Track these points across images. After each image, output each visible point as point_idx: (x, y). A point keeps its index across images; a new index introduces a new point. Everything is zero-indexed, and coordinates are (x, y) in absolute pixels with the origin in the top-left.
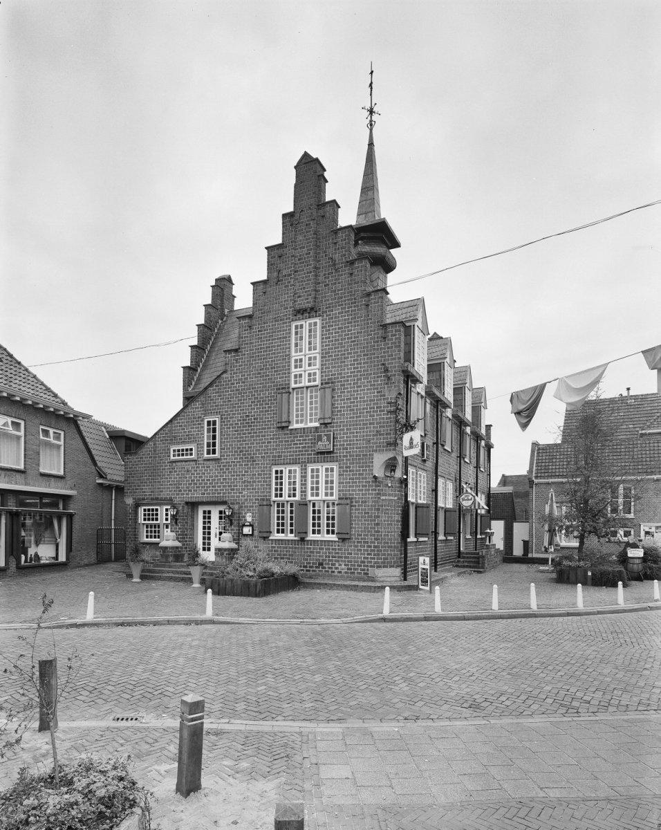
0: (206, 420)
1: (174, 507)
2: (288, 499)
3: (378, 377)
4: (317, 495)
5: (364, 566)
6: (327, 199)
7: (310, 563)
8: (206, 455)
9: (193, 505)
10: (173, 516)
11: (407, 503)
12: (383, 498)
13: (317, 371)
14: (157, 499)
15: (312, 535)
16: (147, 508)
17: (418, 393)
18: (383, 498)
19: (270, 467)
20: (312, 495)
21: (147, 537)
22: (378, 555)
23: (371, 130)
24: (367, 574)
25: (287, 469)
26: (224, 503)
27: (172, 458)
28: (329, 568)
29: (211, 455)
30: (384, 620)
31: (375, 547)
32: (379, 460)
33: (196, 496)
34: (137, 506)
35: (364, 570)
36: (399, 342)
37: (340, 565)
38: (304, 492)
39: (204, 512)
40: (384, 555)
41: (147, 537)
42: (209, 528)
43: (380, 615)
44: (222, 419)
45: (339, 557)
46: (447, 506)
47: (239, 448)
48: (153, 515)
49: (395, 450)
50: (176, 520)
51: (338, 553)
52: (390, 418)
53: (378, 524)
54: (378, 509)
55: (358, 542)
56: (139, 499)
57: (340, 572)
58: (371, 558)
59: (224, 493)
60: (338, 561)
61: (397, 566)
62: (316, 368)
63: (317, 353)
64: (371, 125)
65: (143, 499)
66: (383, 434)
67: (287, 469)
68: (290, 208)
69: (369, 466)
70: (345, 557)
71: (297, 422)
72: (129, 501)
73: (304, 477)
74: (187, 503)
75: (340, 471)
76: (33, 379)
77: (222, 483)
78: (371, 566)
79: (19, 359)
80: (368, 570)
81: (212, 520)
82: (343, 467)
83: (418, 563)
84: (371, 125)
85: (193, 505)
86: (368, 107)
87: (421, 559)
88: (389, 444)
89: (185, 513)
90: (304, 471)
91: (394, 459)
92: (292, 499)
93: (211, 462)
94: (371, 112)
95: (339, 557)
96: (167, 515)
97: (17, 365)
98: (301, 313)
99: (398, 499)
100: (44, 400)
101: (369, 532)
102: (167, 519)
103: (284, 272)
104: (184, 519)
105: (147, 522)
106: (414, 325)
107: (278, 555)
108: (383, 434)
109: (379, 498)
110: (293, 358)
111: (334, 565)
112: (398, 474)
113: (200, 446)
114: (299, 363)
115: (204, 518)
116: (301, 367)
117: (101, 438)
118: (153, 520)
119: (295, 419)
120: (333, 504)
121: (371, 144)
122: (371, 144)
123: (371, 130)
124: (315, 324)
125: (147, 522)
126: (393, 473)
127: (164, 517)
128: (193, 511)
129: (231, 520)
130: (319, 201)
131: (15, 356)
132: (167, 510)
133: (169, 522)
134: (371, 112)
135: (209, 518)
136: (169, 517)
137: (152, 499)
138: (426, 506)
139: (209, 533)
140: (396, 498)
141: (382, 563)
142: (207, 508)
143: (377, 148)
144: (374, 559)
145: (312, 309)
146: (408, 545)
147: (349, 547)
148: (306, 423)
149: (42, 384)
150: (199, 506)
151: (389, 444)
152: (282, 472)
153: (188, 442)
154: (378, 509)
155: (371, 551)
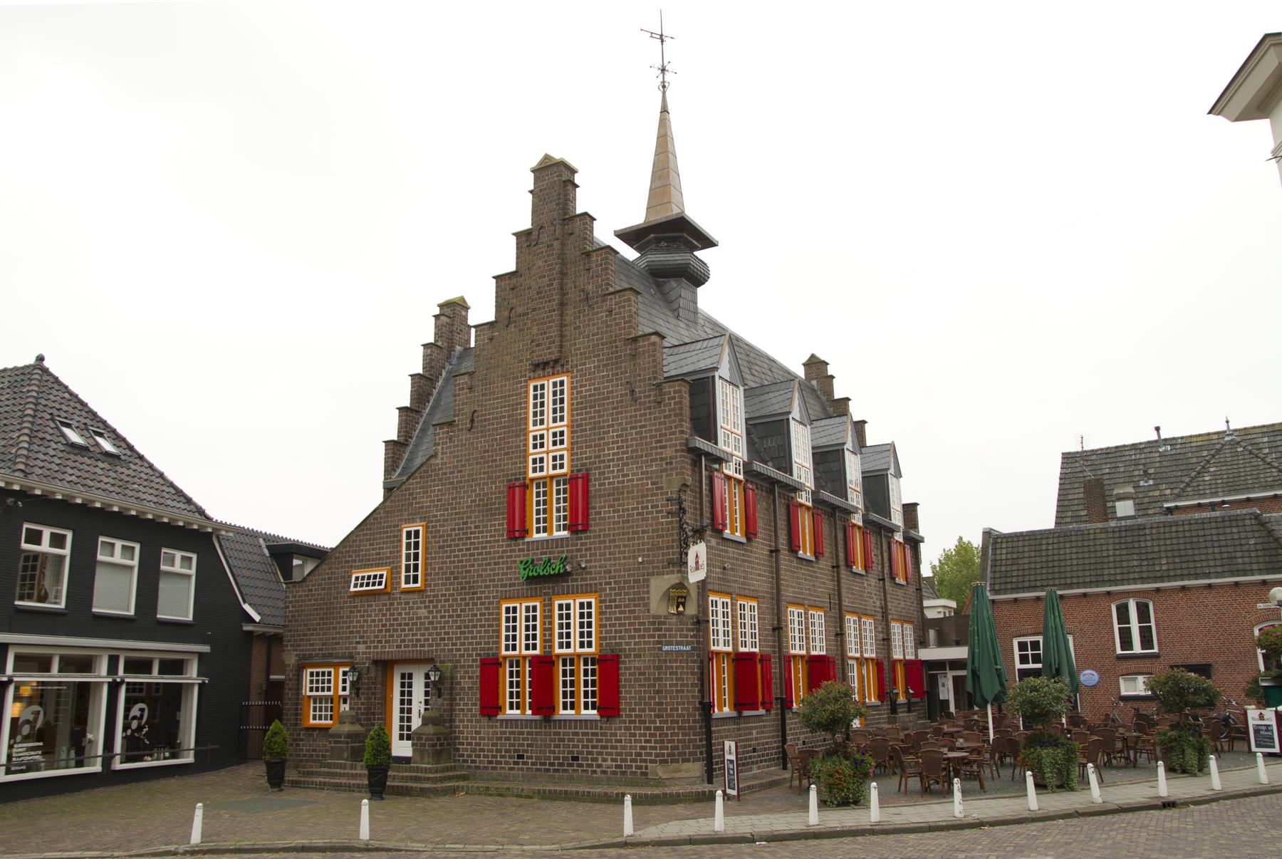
0: (405, 531)
1: (353, 669)
2: (579, 650)
3: (652, 461)
4: (514, 648)
5: (641, 761)
6: (578, 212)
7: (558, 758)
8: (404, 586)
9: (385, 666)
10: (352, 683)
11: (706, 658)
12: (666, 648)
13: (565, 453)
14: (331, 655)
15: (562, 712)
16: (315, 670)
17: (729, 478)
18: (666, 648)
19: (498, 603)
20: (561, 646)
21: (314, 718)
22: (662, 741)
23: (664, 93)
24: (644, 774)
25: (524, 605)
26: (430, 661)
27: (404, 586)
28: (588, 765)
29: (412, 585)
30: (625, 845)
31: (656, 729)
32: (659, 585)
33: (389, 650)
34: (300, 668)
35: (640, 767)
36: (681, 409)
37: (605, 760)
38: (548, 641)
39: (403, 676)
40: (672, 741)
41: (314, 718)
42: (410, 702)
43: (620, 840)
44: (428, 527)
45: (603, 747)
46: (908, 657)
47: (452, 573)
48: (317, 681)
49: (679, 572)
50: (358, 689)
51: (601, 741)
52: (671, 523)
53: (659, 692)
54: (659, 668)
55: (630, 722)
56: (305, 657)
57: (604, 772)
58: (651, 748)
59: (430, 645)
60: (601, 754)
61: (699, 760)
62: (563, 450)
63: (563, 426)
64: (664, 87)
65: (311, 656)
66: (662, 548)
67: (524, 605)
68: (526, 223)
69: (643, 599)
70: (612, 747)
71: (538, 531)
72: (291, 659)
73: (548, 617)
74: (375, 662)
75: (601, 607)
76: (159, 480)
77: (427, 629)
78: (652, 761)
79: (142, 452)
80: (646, 767)
81: (414, 689)
82: (604, 601)
83: (723, 749)
84: (664, 87)
85: (385, 666)
86: (659, 65)
87: (727, 744)
88: (670, 563)
89: (374, 679)
90: (548, 608)
91: (681, 586)
92: (586, 650)
93: (411, 596)
94: (663, 70)
95: (603, 747)
96: (344, 681)
97: (137, 461)
98: (543, 367)
99: (693, 649)
100: (171, 513)
101: (646, 704)
102: (344, 689)
103: (520, 310)
104: (369, 689)
105: (314, 693)
106: (713, 377)
107: (510, 745)
108: (662, 548)
109: (660, 649)
110: (565, 423)
111: (596, 760)
112: (691, 609)
113: (394, 573)
114: (558, 438)
115: (403, 685)
116: (542, 445)
117: (258, 559)
118: (323, 689)
119: (535, 525)
120: (593, 659)
121: (664, 110)
122: (664, 110)
123: (664, 93)
124: (562, 383)
125: (314, 693)
126: (681, 609)
127: (341, 685)
128: (384, 676)
129: (439, 690)
130: (565, 214)
131: (136, 448)
132: (345, 674)
133: (347, 693)
134: (663, 70)
135: (410, 685)
136: (348, 685)
137: (324, 656)
138: (765, 659)
139: (410, 711)
140: (688, 648)
141: (669, 755)
142: (407, 670)
143: (673, 116)
144: (655, 748)
145: (556, 361)
146: (713, 723)
147: (617, 729)
148: (551, 533)
149: (172, 485)
150: (395, 667)
151: (670, 563)
152: (515, 609)
153: (378, 565)
154: (659, 668)
155: (651, 735)
